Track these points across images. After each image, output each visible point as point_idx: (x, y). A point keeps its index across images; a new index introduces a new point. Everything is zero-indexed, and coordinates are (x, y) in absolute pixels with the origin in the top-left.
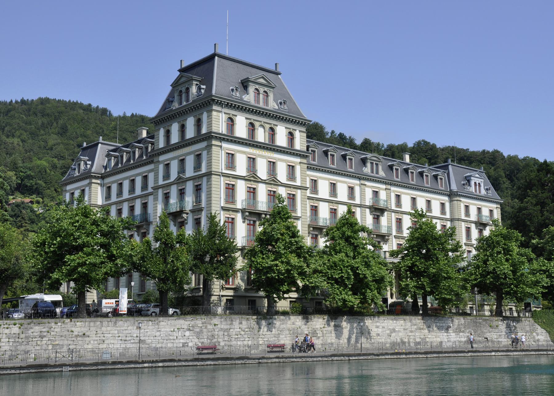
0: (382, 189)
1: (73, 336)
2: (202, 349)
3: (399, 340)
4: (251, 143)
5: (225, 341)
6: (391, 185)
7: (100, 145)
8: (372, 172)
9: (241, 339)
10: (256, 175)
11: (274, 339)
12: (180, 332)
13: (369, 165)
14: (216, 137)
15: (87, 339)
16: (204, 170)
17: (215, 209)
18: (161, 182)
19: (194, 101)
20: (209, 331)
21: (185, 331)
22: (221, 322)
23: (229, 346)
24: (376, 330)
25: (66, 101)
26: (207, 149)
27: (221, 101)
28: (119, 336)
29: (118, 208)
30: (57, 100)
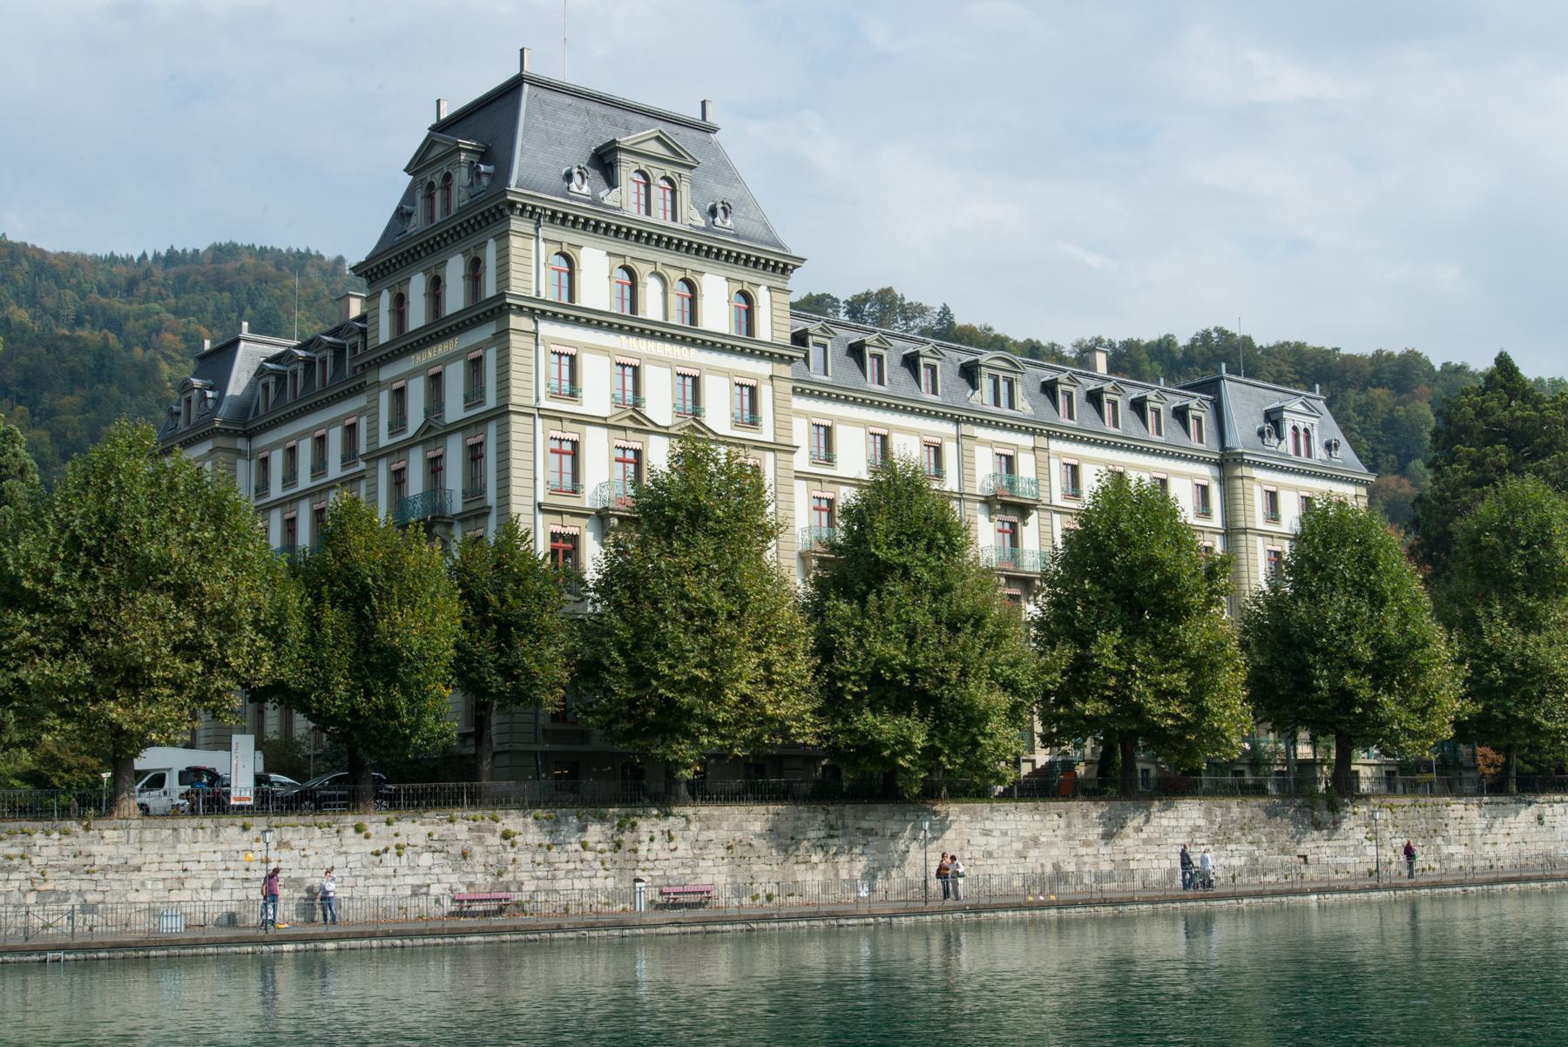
0: (1024, 449)
1: (95, 868)
2: (469, 901)
3: (1049, 869)
4: (629, 324)
5: (538, 878)
6: (1049, 436)
7: (242, 344)
8: (997, 403)
9: (584, 873)
10: (699, 422)
11: (681, 871)
12: (404, 857)
13: (986, 384)
14: (520, 307)
15: (135, 876)
16: (491, 401)
17: (520, 505)
18: (384, 440)
19: (462, 211)
20: (489, 853)
21: (419, 854)
22: (526, 825)
23: (547, 892)
24: (982, 840)
25: (280, 251)
26: (497, 342)
27: (534, 207)
28: (227, 869)
29: (287, 516)
30: (258, 248)
